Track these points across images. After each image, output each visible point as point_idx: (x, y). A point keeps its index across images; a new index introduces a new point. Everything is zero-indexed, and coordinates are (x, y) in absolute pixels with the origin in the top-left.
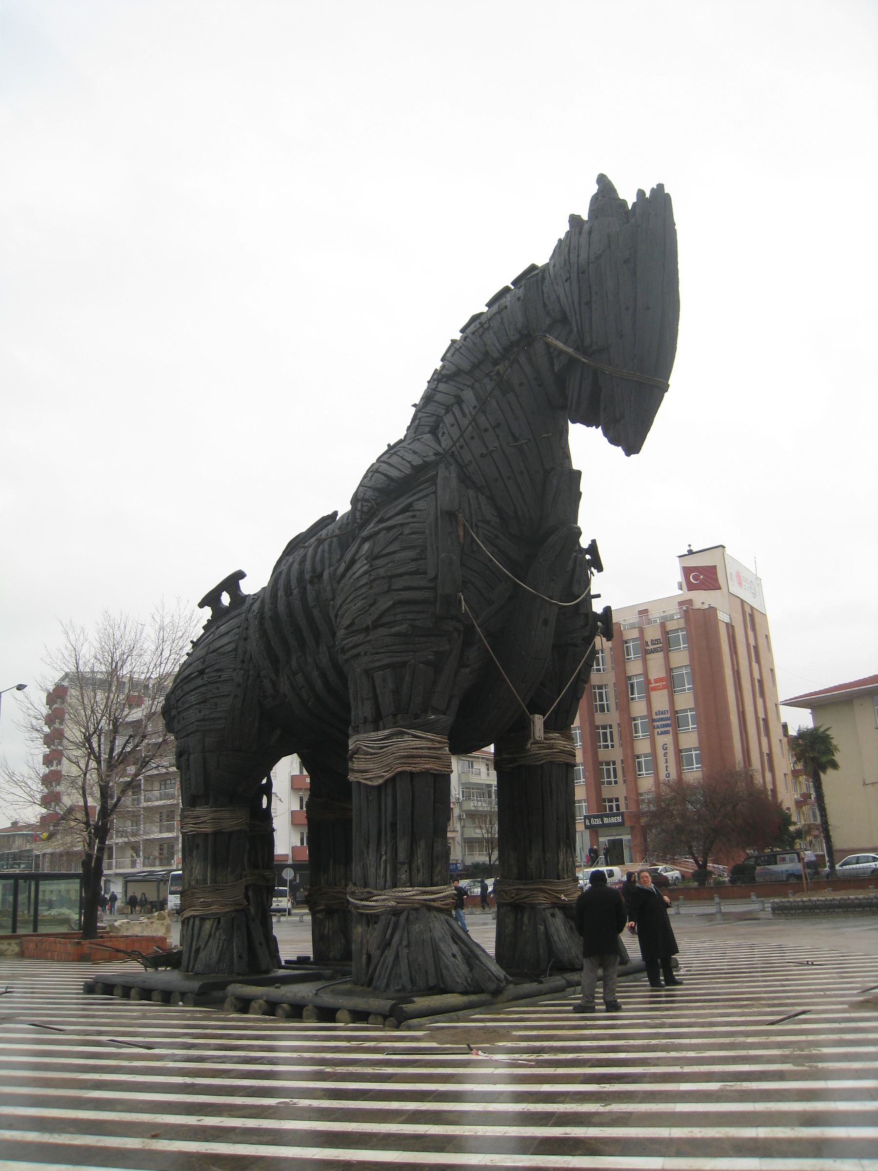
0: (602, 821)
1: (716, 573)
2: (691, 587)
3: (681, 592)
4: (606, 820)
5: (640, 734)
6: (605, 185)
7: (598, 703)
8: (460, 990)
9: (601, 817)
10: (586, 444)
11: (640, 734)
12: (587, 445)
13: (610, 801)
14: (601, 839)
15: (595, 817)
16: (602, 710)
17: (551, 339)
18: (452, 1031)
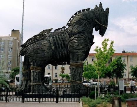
6: (101, 4)
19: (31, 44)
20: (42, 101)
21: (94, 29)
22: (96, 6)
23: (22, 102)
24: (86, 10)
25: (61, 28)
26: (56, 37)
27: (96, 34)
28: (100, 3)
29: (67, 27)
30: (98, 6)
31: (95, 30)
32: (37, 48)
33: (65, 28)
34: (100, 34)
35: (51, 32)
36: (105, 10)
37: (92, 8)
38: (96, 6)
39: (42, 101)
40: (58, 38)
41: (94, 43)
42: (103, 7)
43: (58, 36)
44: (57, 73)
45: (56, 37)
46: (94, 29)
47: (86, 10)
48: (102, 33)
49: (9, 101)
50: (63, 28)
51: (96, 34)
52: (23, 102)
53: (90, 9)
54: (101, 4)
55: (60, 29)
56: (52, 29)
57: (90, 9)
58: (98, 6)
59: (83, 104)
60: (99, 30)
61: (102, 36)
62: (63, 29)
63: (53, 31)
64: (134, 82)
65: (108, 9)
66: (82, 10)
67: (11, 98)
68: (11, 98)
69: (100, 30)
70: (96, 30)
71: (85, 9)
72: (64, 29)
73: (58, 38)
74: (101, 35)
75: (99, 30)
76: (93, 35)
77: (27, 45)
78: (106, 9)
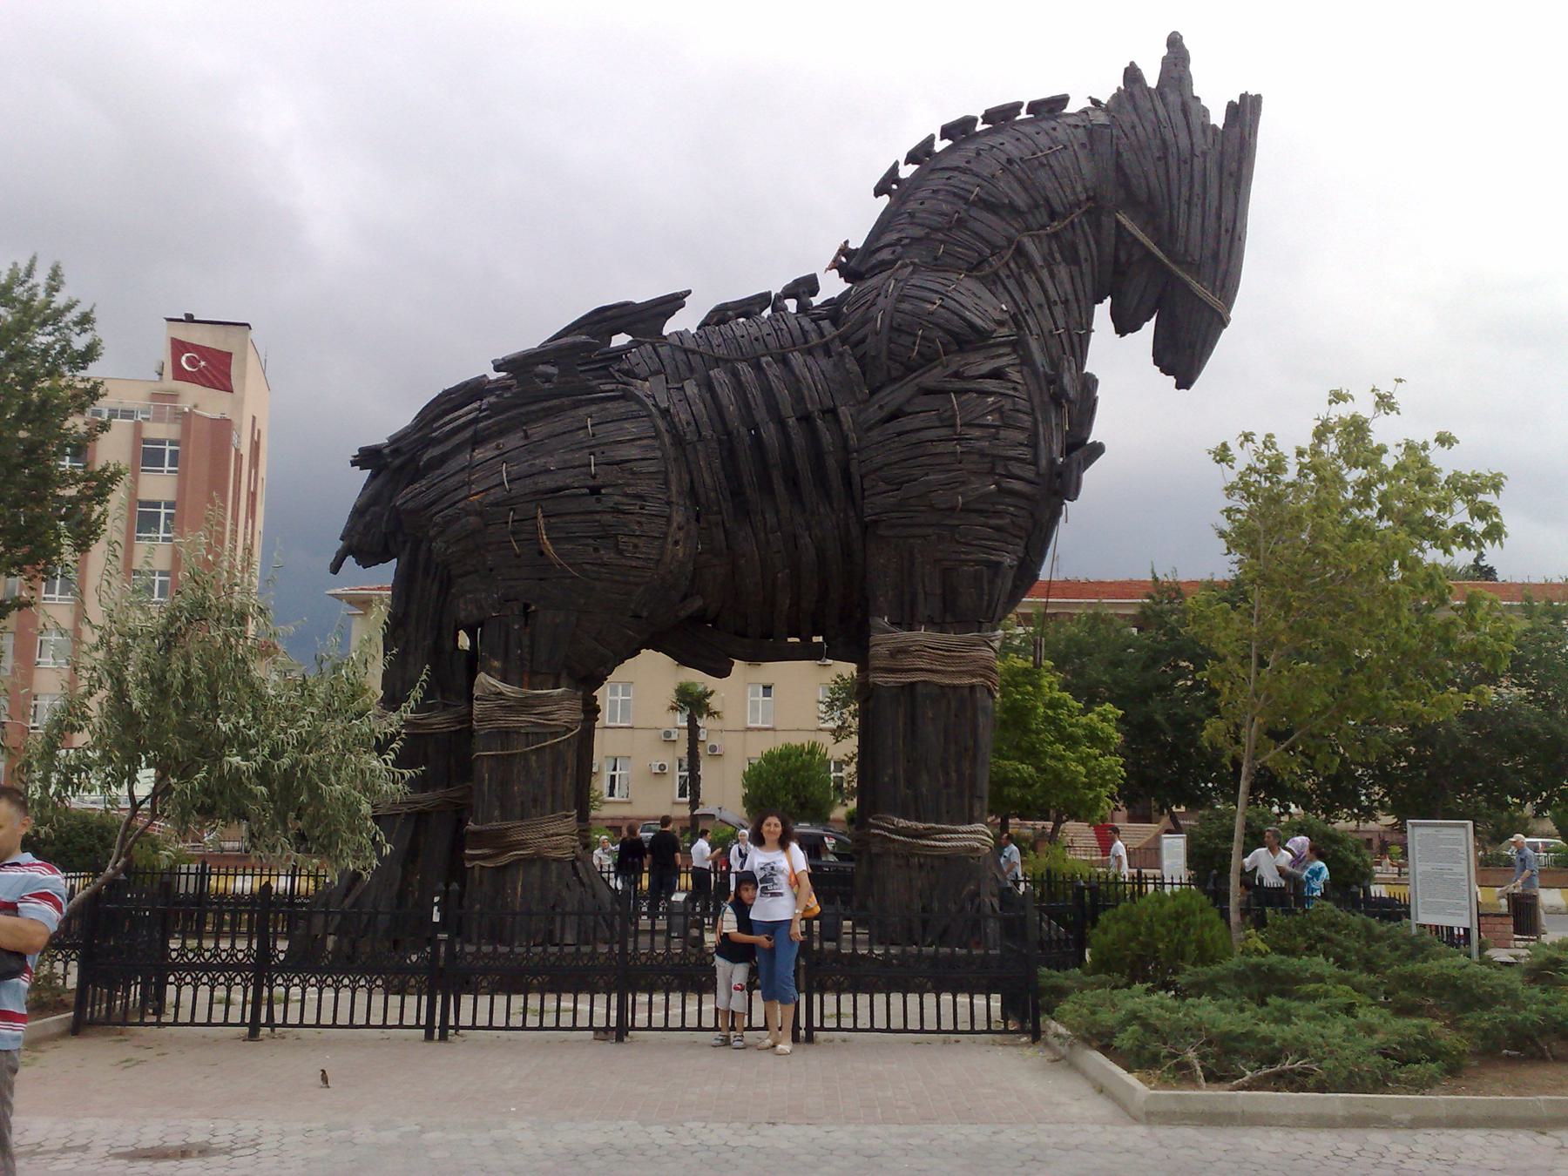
1: (229, 366)
2: (179, 374)
17: (1124, 219)
19: (477, 441)
21: (1102, 312)
22: (1132, 75)
23: (429, 1037)
25: (776, 289)
26: (739, 387)
27: (1119, 359)
28: (1175, 42)
29: (832, 286)
30: (1152, 80)
31: (1115, 315)
32: (547, 482)
33: (814, 291)
34: (1158, 361)
35: (670, 327)
36: (1218, 118)
37: (1089, 83)
38: (1132, 75)
40: (755, 393)
41: (1098, 449)
43: (757, 367)
45: (739, 387)
46: (1102, 312)
47: (980, 127)
48: (1182, 357)
49: (457, 1027)
50: (789, 292)
51: (1119, 359)
52: (810, 1039)
53: (1063, 100)
55: (763, 299)
56: (673, 303)
57: (1071, 108)
58: (1152, 80)
59: (154, 1019)
60: (1149, 327)
61: (1184, 383)
63: (683, 322)
64: (55, 914)
65: (1245, 111)
66: (989, 116)
67: (220, 993)
68: (220, 993)
70: (1125, 324)
71: (1016, 107)
73: (755, 393)
74: (1166, 370)
75: (1149, 327)
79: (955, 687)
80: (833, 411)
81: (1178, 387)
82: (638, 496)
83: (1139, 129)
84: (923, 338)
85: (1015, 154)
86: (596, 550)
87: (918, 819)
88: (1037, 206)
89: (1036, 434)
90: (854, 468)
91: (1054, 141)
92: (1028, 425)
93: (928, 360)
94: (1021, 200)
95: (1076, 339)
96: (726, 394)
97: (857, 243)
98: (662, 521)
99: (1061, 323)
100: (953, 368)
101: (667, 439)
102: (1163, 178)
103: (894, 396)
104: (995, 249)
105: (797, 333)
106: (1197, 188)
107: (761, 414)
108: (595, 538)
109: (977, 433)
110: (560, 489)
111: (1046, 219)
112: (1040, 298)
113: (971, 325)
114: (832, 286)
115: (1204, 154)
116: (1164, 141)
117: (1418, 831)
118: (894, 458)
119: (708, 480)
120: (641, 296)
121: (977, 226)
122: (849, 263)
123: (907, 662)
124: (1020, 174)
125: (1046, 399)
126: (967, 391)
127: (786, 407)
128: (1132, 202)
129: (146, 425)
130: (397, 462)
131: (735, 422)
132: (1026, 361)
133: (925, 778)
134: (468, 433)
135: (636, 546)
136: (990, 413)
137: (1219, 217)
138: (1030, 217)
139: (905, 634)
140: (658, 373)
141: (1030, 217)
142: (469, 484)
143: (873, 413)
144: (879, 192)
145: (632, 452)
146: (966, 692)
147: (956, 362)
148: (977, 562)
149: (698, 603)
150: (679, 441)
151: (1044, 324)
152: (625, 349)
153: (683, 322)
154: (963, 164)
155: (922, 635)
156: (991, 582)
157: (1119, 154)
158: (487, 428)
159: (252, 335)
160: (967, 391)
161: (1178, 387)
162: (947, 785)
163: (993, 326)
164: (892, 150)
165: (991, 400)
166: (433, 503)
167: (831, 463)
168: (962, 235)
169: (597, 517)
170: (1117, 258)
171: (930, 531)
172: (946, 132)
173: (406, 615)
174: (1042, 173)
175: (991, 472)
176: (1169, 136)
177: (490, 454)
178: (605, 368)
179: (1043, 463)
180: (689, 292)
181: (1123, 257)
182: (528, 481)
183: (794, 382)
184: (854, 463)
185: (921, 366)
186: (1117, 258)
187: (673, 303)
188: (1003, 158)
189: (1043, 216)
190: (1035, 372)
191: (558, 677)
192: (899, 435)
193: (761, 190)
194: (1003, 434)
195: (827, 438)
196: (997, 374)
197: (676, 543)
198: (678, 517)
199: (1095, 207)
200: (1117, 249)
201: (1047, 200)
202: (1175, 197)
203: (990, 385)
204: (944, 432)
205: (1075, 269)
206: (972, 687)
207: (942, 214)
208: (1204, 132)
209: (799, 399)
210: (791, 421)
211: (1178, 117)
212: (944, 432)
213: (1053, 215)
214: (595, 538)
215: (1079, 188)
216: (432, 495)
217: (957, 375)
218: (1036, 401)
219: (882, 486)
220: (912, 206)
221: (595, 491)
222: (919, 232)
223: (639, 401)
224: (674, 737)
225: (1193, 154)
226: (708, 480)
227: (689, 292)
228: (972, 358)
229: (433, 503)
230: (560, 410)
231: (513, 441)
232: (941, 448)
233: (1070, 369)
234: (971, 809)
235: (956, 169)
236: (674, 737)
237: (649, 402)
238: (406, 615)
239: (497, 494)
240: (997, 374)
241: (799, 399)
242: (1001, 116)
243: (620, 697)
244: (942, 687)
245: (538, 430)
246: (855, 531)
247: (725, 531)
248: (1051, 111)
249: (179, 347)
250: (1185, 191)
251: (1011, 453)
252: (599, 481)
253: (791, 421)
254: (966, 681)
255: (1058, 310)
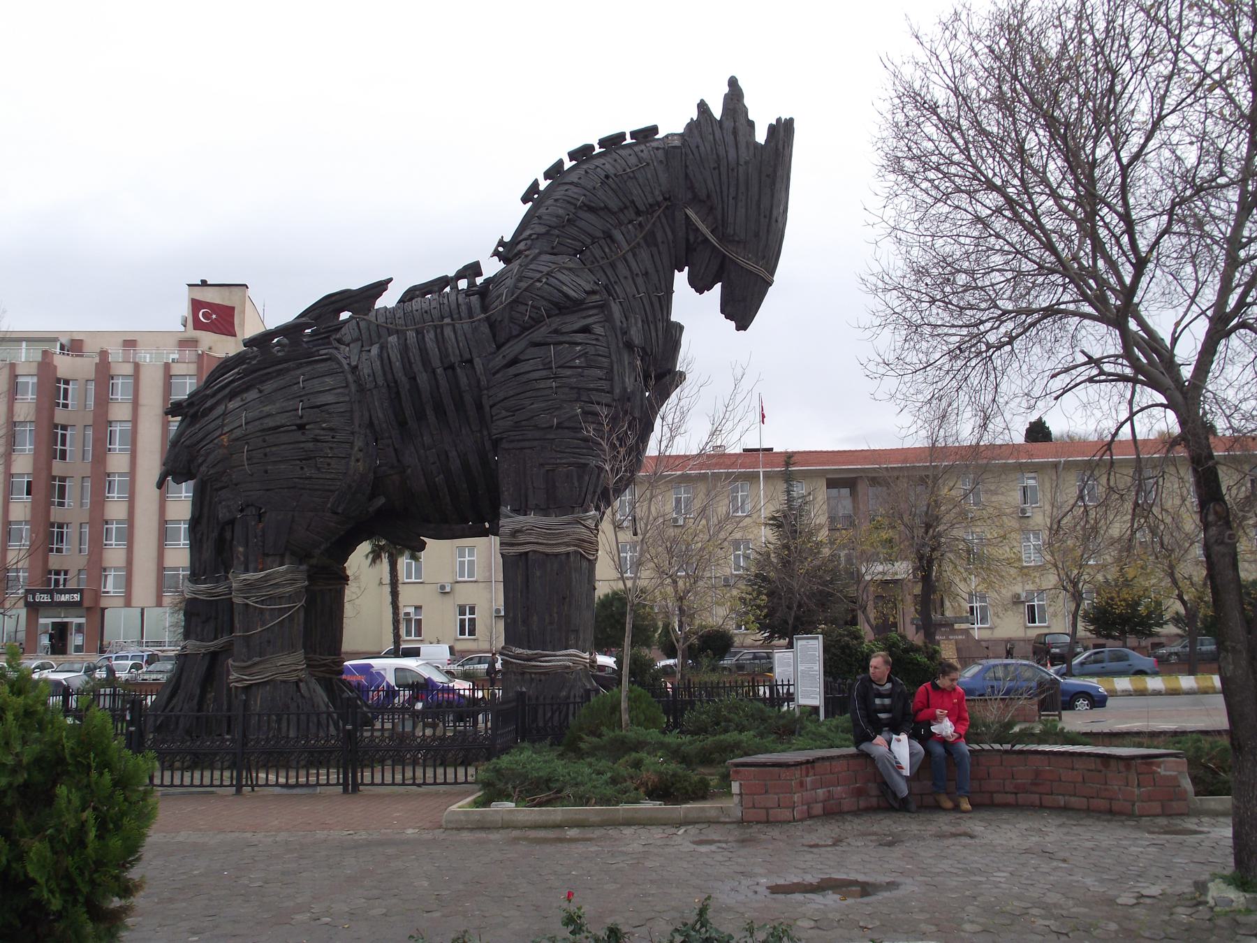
0: (52, 598)
1: (233, 316)
2: (198, 325)
3: (182, 329)
4: (58, 598)
5: (115, 495)
6: (735, 94)
7: (59, 447)
8: (1162, 738)
9: (50, 593)
10: (694, 308)
11: (115, 495)
12: (694, 308)
13: (58, 573)
14: (42, 621)
15: (42, 592)
16: (63, 457)
17: (690, 212)
18: (1079, 764)
19: (232, 396)
20: (367, 780)
21: (681, 278)
22: (703, 107)
24: (629, 140)
25: (451, 274)
28: (733, 83)
29: (492, 267)
30: (717, 112)
32: (270, 423)
34: (722, 312)
35: (380, 303)
36: (761, 136)
38: (703, 107)
39: (367, 780)
42: (750, 117)
44: (472, 611)
46: (681, 278)
47: (598, 150)
50: (461, 275)
53: (654, 130)
54: (735, 94)
55: (444, 281)
56: (380, 287)
58: (717, 112)
60: (718, 287)
61: (742, 325)
62: (463, 284)
63: (388, 300)
65: (783, 131)
66: (602, 143)
69: (722, 287)
70: (700, 285)
71: (622, 136)
72: (471, 284)
75: (718, 287)
76: (674, 318)
77: (208, 404)
78: (772, 130)
79: (556, 555)
80: (470, 361)
81: (738, 329)
82: (331, 429)
83: (702, 148)
84: (532, 306)
85: (612, 171)
86: (302, 468)
87: (529, 648)
88: (626, 207)
89: (612, 370)
90: (485, 400)
91: (640, 160)
92: (606, 365)
93: (537, 321)
94: (614, 204)
95: (655, 301)
96: (395, 355)
97: (507, 239)
98: (347, 446)
99: (642, 288)
100: (554, 326)
101: (353, 387)
102: (717, 182)
103: (511, 350)
104: (594, 240)
105: (454, 306)
106: (742, 188)
107: (418, 366)
108: (301, 460)
109: (568, 372)
110: (279, 427)
111: (633, 216)
112: (626, 272)
113: (566, 296)
114: (492, 267)
115: (746, 163)
116: (718, 156)
117: (800, 643)
118: (511, 393)
119: (380, 415)
120: (355, 285)
121: (582, 224)
122: (506, 251)
123: (521, 539)
124: (614, 186)
125: (621, 345)
126: (561, 343)
127: (436, 362)
128: (696, 200)
129: (173, 365)
130: (192, 411)
131: (400, 375)
132: (609, 319)
133: (535, 618)
134: (227, 390)
135: (329, 464)
136: (578, 358)
137: (759, 207)
138: (622, 216)
139: (521, 518)
140: (357, 340)
141: (622, 216)
142: (223, 426)
143: (499, 361)
144: (525, 200)
145: (329, 398)
146: (563, 557)
147: (556, 322)
148: (570, 465)
149: (381, 501)
150: (361, 389)
151: (628, 290)
152: (346, 322)
153: (388, 300)
154: (576, 180)
155: (531, 519)
156: (580, 478)
157: (686, 166)
158: (239, 386)
159: (250, 292)
160: (561, 343)
161: (738, 329)
162: (551, 623)
163: (584, 295)
164: (535, 171)
165: (578, 348)
166: (202, 440)
167: (468, 398)
168: (573, 231)
169: (302, 445)
170: (688, 240)
171: (535, 443)
172: (572, 155)
173: (200, 516)
174: (630, 183)
175: (578, 400)
176: (722, 152)
177: (237, 405)
178: (328, 337)
179: (617, 391)
180: (391, 280)
181: (692, 238)
182: (257, 423)
183: (440, 340)
184: (485, 397)
185: (532, 327)
186: (688, 240)
187: (380, 287)
188: (603, 175)
189: (630, 214)
190: (614, 328)
191: (282, 556)
192: (516, 375)
193: (435, 203)
194: (586, 372)
195: (464, 381)
196: (586, 330)
197: (358, 460)
198: (359, 443)
199: (669, 203)
200: (687, 233)
201: (633, 202)
202: (725, 194)
203: (579, 337)
204: (544, 373)
205: (654, 249)
206: (568, 554)
207: (557, 216)
208: (747, 147)
209: (444, 355)
210: (439, 371)
211: (730, 139)
212: (544, 373)
213: (638, 213)
214: (301, 460)
215: (657, 193)
216: (200, 435)
217: (556, 331)
218: (613, 347)
219: (504, 413)
220: (542, 210)
221: (301, 427)
222: (543, 230)
223: (339, 363)
224: (448, 589)
225: (738, 164)
226: (380, 415)
227: (391, 280)
228: (568, 318)
229: (202, 440)
230: (288, 370)
231: (253, 395)
232: (542, 385)
233: (636, 323)
234: (567, 640)
235: (572, 183)
236: (448, 589)
237: (344, 362)
238: (200, 516)
239: (238, 433)
240: (586, 330)
241: (444, 355)
242: (612, 142)
243: (467, 559)
244: (547, 555)
245: (268, 387)
246: (488, 445)
247: (395, 450)
248: (646, 137)
249: (196, 305)
250: (732, 190)
251: (592, 386)
252: (304, 420)
253: (439, 371)
254: (563, 549)
255: (640, 281)
